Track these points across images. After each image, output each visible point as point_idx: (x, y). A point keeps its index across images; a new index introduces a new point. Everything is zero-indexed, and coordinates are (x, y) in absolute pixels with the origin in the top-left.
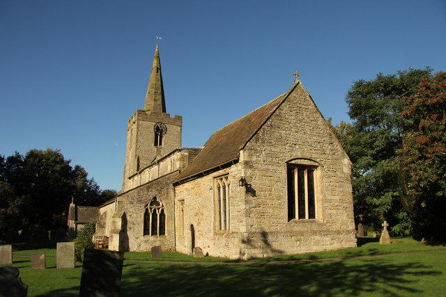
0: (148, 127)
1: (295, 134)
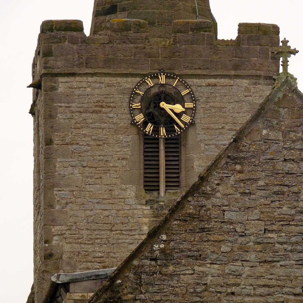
0: (99, 107)
1: (261, 269)
